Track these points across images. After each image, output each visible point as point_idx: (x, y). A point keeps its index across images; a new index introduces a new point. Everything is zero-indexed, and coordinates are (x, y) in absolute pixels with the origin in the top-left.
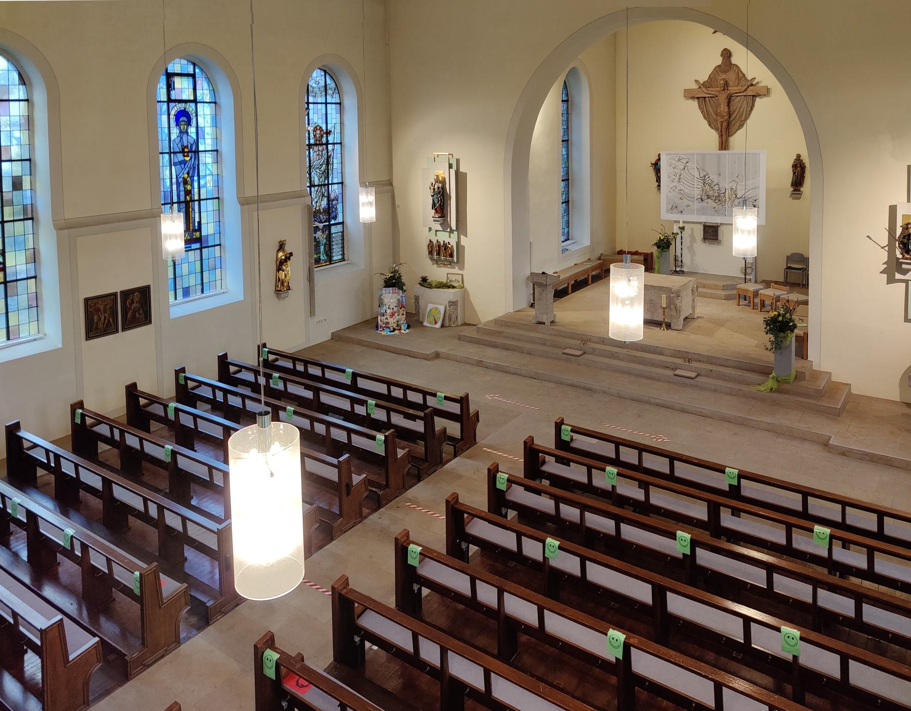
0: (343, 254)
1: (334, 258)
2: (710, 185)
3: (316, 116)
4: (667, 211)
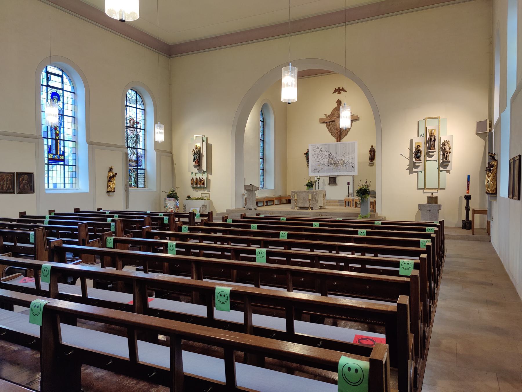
0: (145, 185)
1: (140, 186)
2: (332, 158)
3: (131, 113)
4: (312, 172)
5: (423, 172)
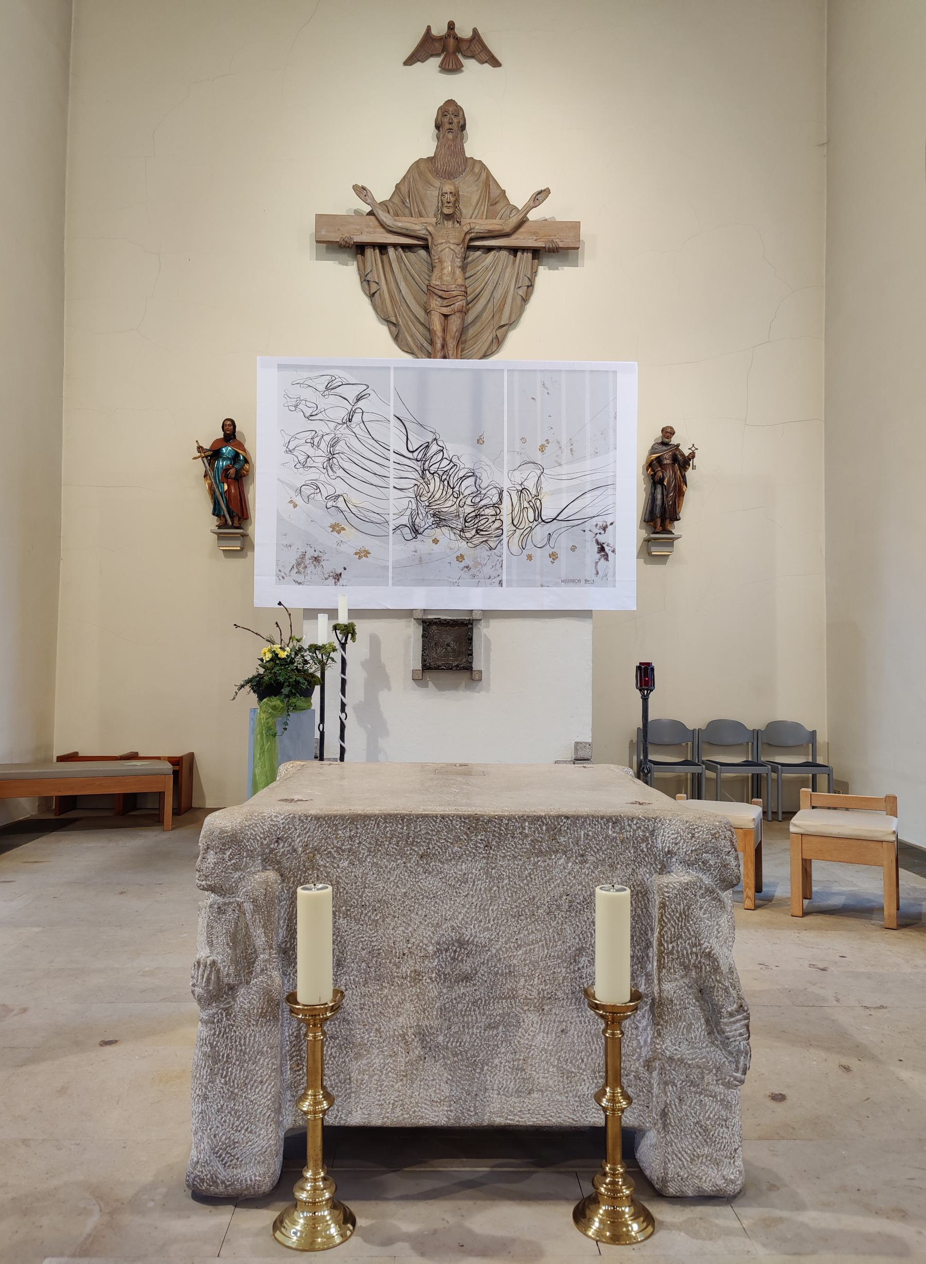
4: (281, 577)
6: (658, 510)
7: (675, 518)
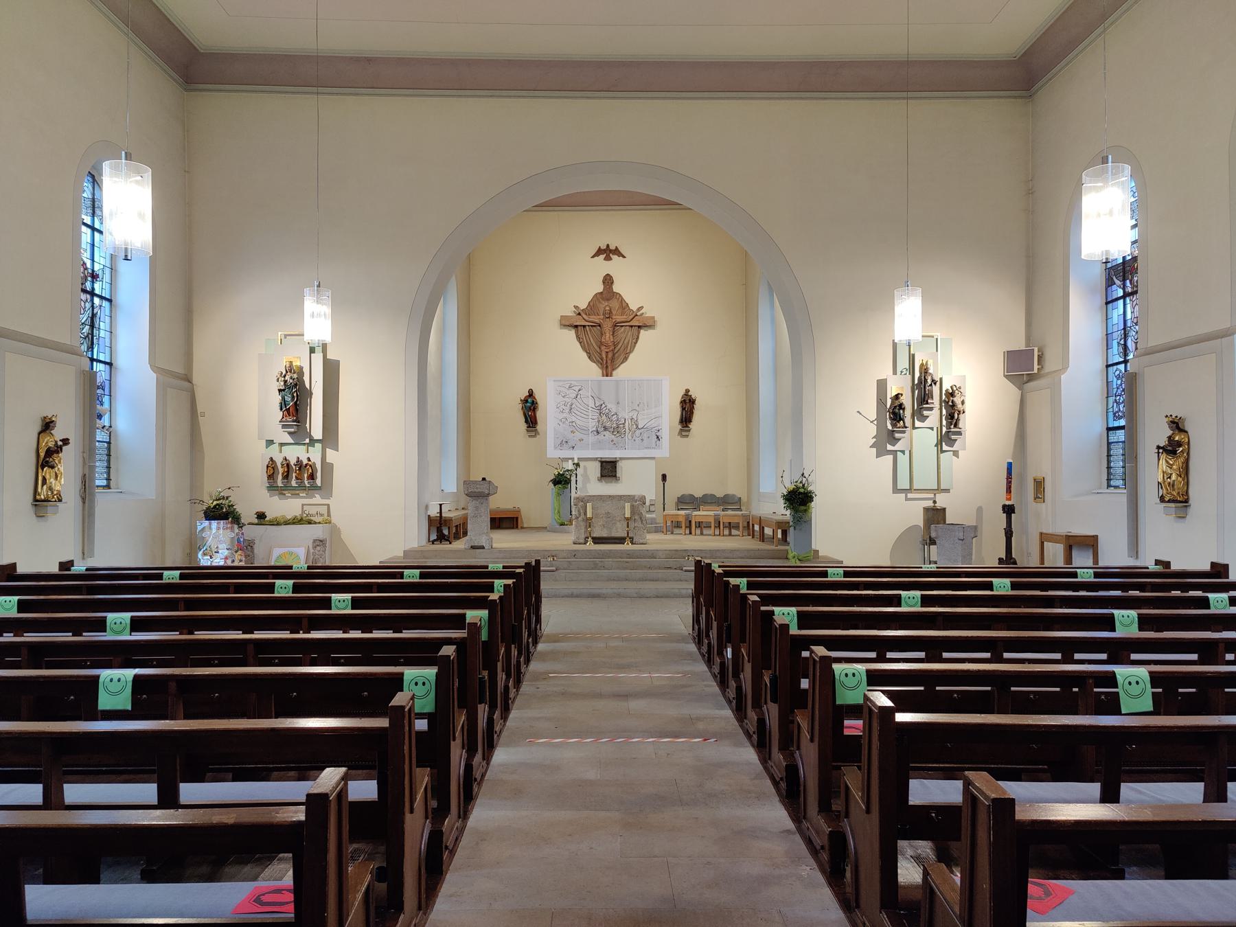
0: (108, 479)
5: (907, 453)
6: (684, 420)
7: (690, 421)
